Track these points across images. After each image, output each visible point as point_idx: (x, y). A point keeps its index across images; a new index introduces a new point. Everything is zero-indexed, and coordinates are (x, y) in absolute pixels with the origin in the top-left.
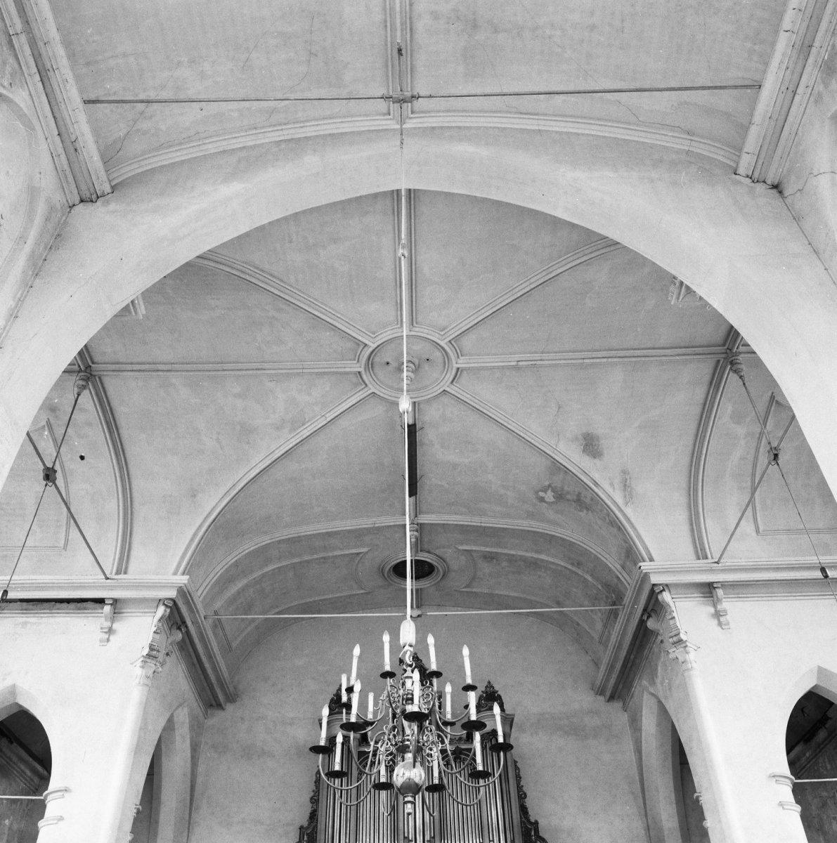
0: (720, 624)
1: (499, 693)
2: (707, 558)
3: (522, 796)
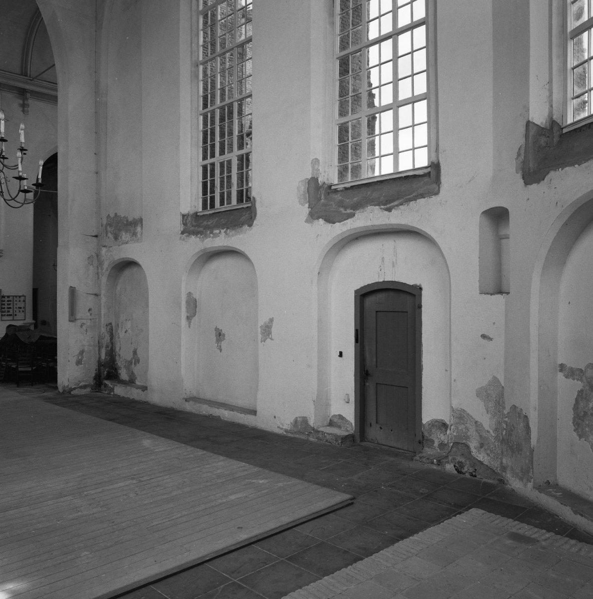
0: (23, 111)
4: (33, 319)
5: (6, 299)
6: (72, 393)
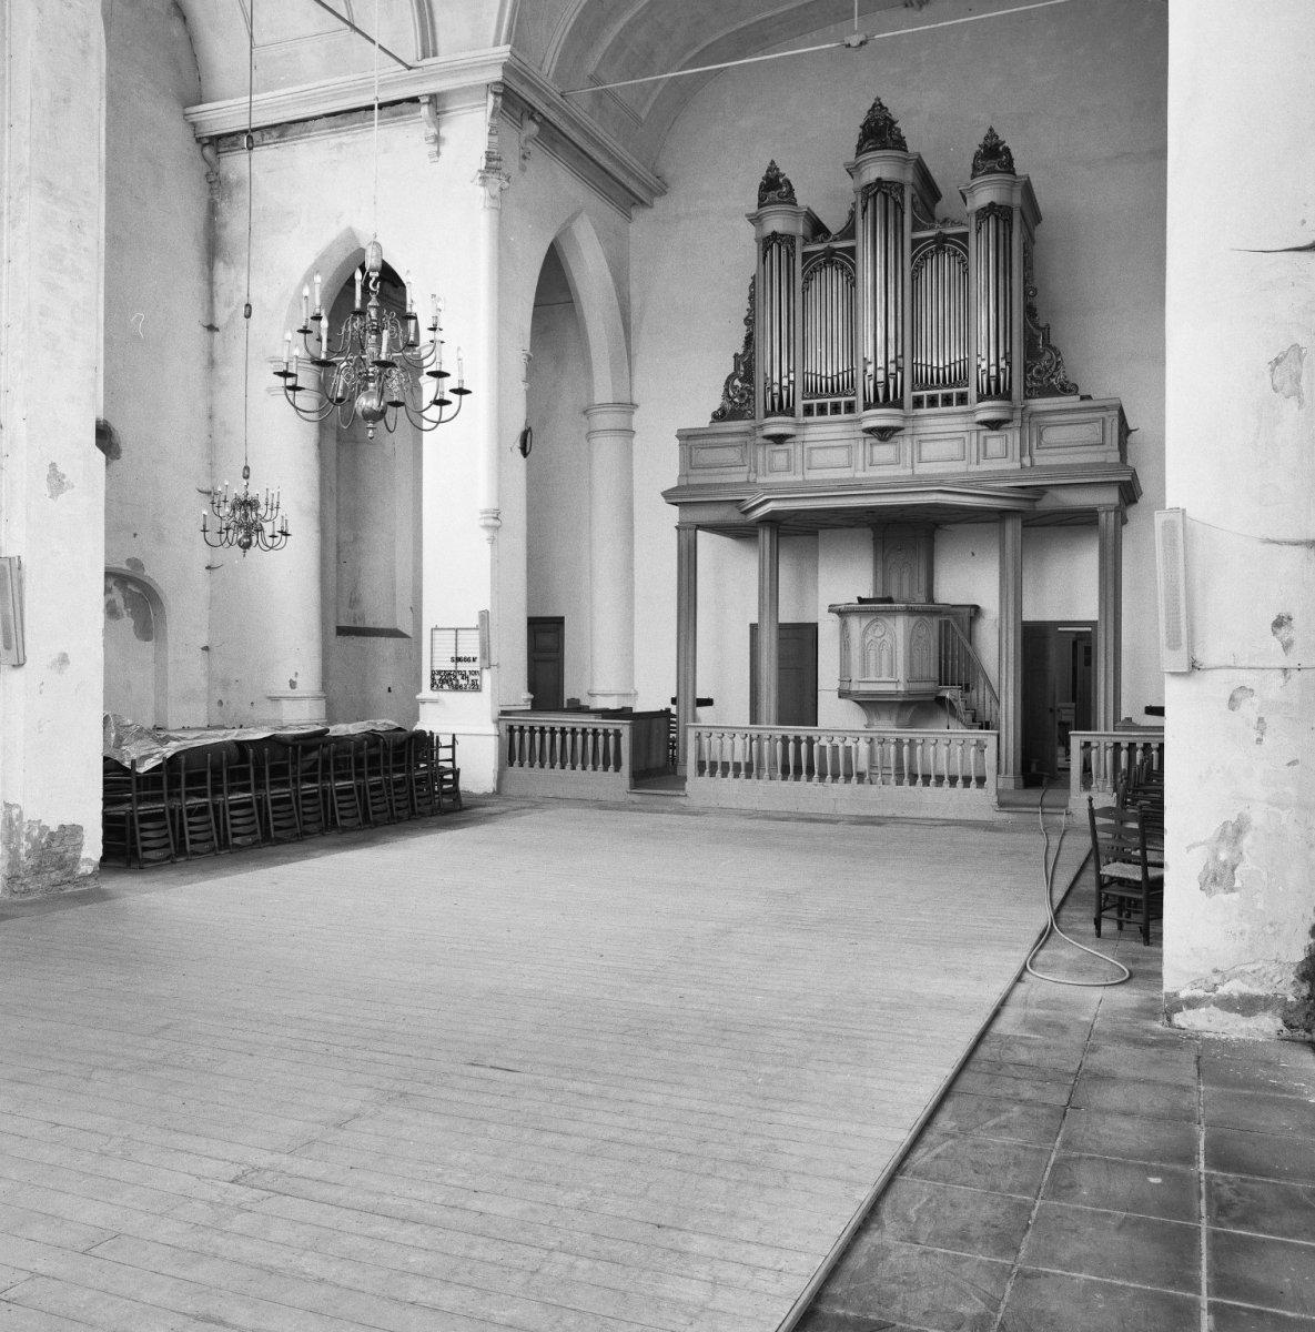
1: (1006, 144)
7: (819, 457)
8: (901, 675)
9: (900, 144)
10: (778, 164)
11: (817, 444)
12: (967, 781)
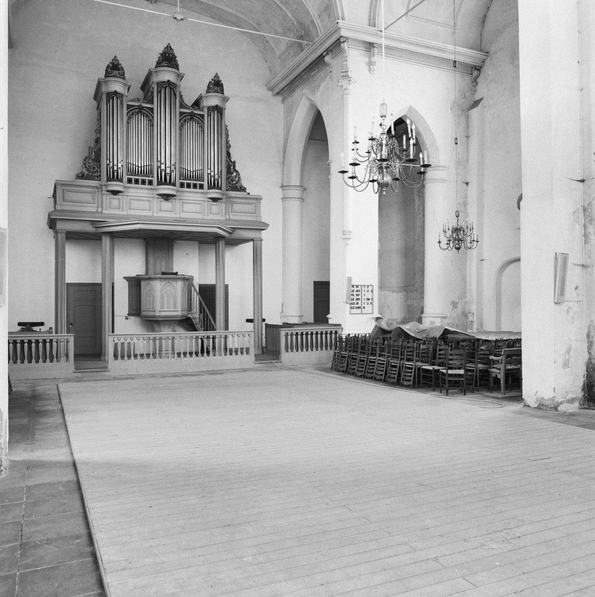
0: (370, 70)
2: (375, 26)
3: (228, 146)
4: (379, 313)
5: (355, 289)
6: (559, 409)
7: (135, 204)
8: (179, 308)
9: (176, 67)
10: (118, 58)
11: (133, 198)
12: (154, 355)
